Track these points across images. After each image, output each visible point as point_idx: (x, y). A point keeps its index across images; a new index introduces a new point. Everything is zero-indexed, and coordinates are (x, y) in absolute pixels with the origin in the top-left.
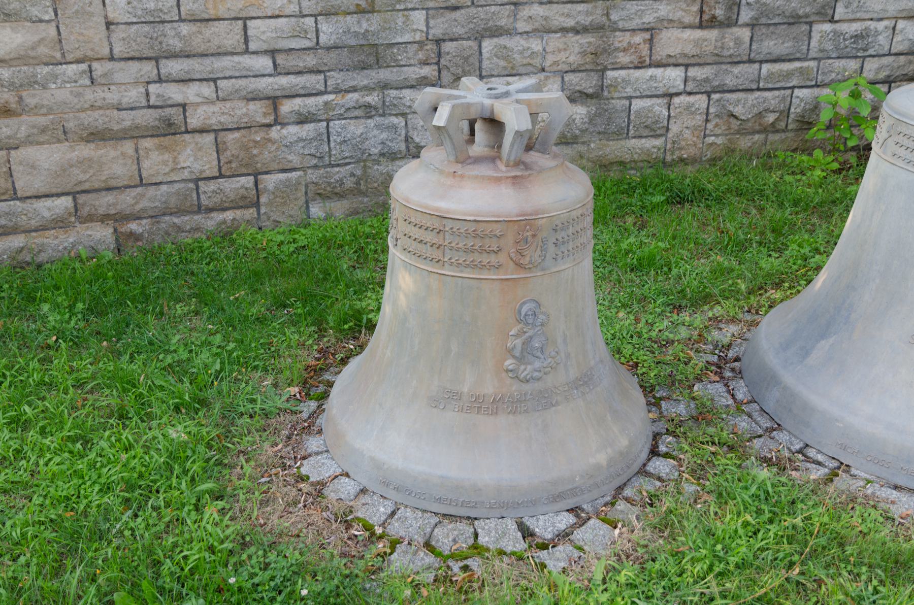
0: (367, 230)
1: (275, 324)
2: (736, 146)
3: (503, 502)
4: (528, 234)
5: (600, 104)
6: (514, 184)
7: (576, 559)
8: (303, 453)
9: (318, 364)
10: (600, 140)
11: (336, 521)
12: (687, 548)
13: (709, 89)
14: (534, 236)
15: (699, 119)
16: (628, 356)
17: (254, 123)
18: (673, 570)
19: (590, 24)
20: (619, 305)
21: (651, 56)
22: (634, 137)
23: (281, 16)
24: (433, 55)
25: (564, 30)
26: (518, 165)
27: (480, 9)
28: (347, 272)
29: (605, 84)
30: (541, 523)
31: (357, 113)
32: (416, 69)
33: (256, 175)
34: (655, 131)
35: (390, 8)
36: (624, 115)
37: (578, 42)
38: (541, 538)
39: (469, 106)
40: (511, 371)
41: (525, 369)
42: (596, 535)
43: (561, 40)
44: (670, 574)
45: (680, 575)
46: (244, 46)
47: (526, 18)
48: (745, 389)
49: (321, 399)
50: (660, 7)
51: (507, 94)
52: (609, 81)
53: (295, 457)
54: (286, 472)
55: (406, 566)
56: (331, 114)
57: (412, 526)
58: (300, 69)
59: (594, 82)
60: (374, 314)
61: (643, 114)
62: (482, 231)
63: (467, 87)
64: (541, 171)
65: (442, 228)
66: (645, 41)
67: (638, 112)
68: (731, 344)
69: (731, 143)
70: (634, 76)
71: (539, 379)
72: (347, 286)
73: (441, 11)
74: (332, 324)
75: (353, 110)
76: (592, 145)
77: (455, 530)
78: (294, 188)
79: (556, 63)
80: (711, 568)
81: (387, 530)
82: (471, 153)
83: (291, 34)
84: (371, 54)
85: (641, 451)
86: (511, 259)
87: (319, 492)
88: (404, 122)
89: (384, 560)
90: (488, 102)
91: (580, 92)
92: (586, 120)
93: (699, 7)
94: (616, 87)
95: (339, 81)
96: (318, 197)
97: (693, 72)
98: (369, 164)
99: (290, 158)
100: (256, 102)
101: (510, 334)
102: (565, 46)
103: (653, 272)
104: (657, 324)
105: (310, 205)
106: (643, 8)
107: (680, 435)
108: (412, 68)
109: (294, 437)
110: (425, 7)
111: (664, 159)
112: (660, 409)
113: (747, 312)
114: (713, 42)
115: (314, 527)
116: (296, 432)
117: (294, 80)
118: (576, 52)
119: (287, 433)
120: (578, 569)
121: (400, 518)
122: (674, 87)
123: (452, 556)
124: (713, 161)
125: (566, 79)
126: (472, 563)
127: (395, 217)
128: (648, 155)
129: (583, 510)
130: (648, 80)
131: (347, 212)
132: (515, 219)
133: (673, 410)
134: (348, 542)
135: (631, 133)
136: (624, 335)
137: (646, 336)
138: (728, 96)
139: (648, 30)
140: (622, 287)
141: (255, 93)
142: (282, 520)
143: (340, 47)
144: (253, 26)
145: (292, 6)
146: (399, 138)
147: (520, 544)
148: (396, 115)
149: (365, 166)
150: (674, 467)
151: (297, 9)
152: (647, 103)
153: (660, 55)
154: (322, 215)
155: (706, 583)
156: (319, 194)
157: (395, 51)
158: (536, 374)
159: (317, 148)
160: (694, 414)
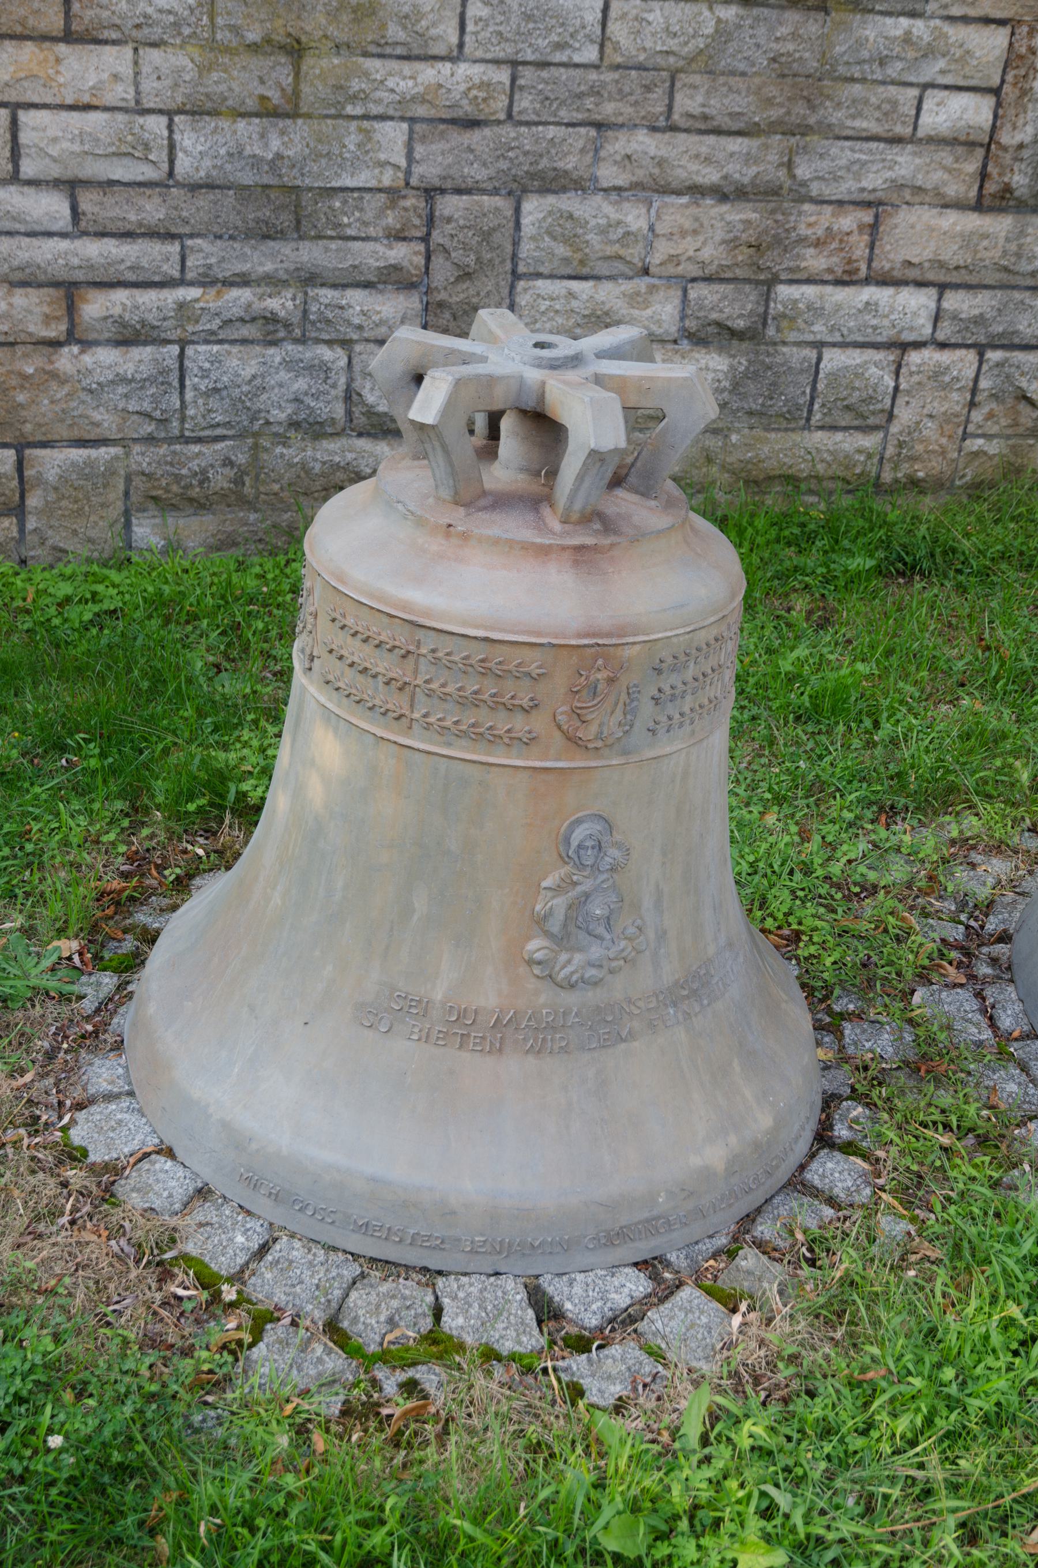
0: (251, 583)
1: (37, 790)
2: (1025, 461)
3: (501, 1242)
4: (599, 676)
5: (757, 353)
6: (576, 563)
7: (648, 1380)
8: (77, 1094)
9: (124, 889)
10: (751, 428)
11: (138, 1262)
12: (883, 1372)
13: (982, 339)
14: (611, 681)
15: (957, 400)
16: (780, 916)
17: (23, 336)
18: (848, 1420)
19: (753, 183)
20: (768, 796)
21: (870, 260)
22: (821, 428)
23: (96, 108)
24: (417, 221)
25: (696, 191)
26: (590, 521)
27: (523, 129)
28: (202, 680)
29: (771, 311)
30: (578, 1290)
31: (246, 331)
32: (380, 248)
33: (21, 447)
34: (865, 418)
35: (333, 111)
36: (805, 379)
37: (722, 219)
38: (576, 1324)
39: (491, 381)
40: (539, 963)
41: (569, 962)
42: (693, 1325)
43: (688, 212)
44: (844, 1430)
45: (864, 1433)
46: (10, 167)
47: (618, 158)
48: (1018, 1007)
49: (127, 969)
50: (899, 159)
51: (575, 361)
52: (779, 306)
53: (61, 1104)
54: (37, 1140)
55: (282, 1376)
56: (190, 328)
57: (301, 1282)
58: (128, 227)
59: (749, 306)
60: (252, 782)
61: (844, 382)
62: (500, 663)
63: (490, 332)
64: (640, 536)
65: (412, 648)
66: (861, 228)
67: (834, 377)
68: (992, 902)
69: (1017, 456)
70: (833, 299)
71: (596, 983)
72: (201, 714)
73: (442, 127)
74: (160, 799)
75: (238, 324)
76: (734, 438)
77: (393, 1297)
78: (100, 480)
79: (674, 259)
80: (929, 1422)
81: (248, 1290)
82: (489, 485)
83: (113, 149)
84: (283, 207)
85: (796, 1140)
86: (559, 727)
87: (106, 1190)
88: (346, 360)
89: (237, 1360)
90: (533, 375)
91: (718, 324)
92: (726, 384)
93: (980, 164)
94: (793, 319)
95: (213, 260)
96: (151, 505)
97: (953, 301)
98: (265, 442)
99: (97, 416)
100: (29, 290)
101: (544, 884)
102: (697, 225)
103: (841, 728)
104: (845, 847)
105: (134, 521)
106: (864, 157)
107: (879, 1103)
108: (370, 246)
109: (61, 1055)
110: (409, 114)
111: (878, 477)
112: (840, 1041)
113: (1029, 830)
114: (1001, 241)
115: (88, 1272)
116: (65, 1046)
117: (114, 251)
118: (718, 238)
119: (46, 1044)
120: (652, 1404)
121: (278, 1262)
122: (911, 329)
123: (384, 1357)
124: (977, 489)
125: (692, 294)
126: (429, 1376)
127: (312, 609)
128: (847, 468)
129: (668, 1265)
130: (860, 311)
131: (211, 540)
132: (573, 642)
133: (868, 1045)
134: (161, 1311)
135: (817, 417)
136: (776, 868)
137: (820, 872)
138: (1019, 356)
139: (869, 204)
140: (776, 757)
141: (28, 271)
142: (19, 1253)
143: (218, 187)
144: (31, 124)
145: (120, 88)
146: (333, 392)
147: (531, 1336)
148: (329, 343)
149: (256, 446)
150: (864, 1174)
151: (131, 95)
152: (854, 358)
153: (888, 260)
154: (156, 541)
155: (917, 1454)
156: (153, 498)
157: (337, 204)
158: (591, 972)
159: (155, 400)
160: (912, 1058)
